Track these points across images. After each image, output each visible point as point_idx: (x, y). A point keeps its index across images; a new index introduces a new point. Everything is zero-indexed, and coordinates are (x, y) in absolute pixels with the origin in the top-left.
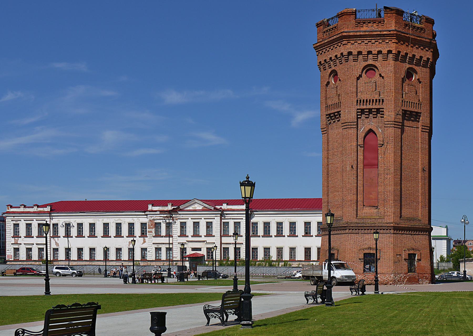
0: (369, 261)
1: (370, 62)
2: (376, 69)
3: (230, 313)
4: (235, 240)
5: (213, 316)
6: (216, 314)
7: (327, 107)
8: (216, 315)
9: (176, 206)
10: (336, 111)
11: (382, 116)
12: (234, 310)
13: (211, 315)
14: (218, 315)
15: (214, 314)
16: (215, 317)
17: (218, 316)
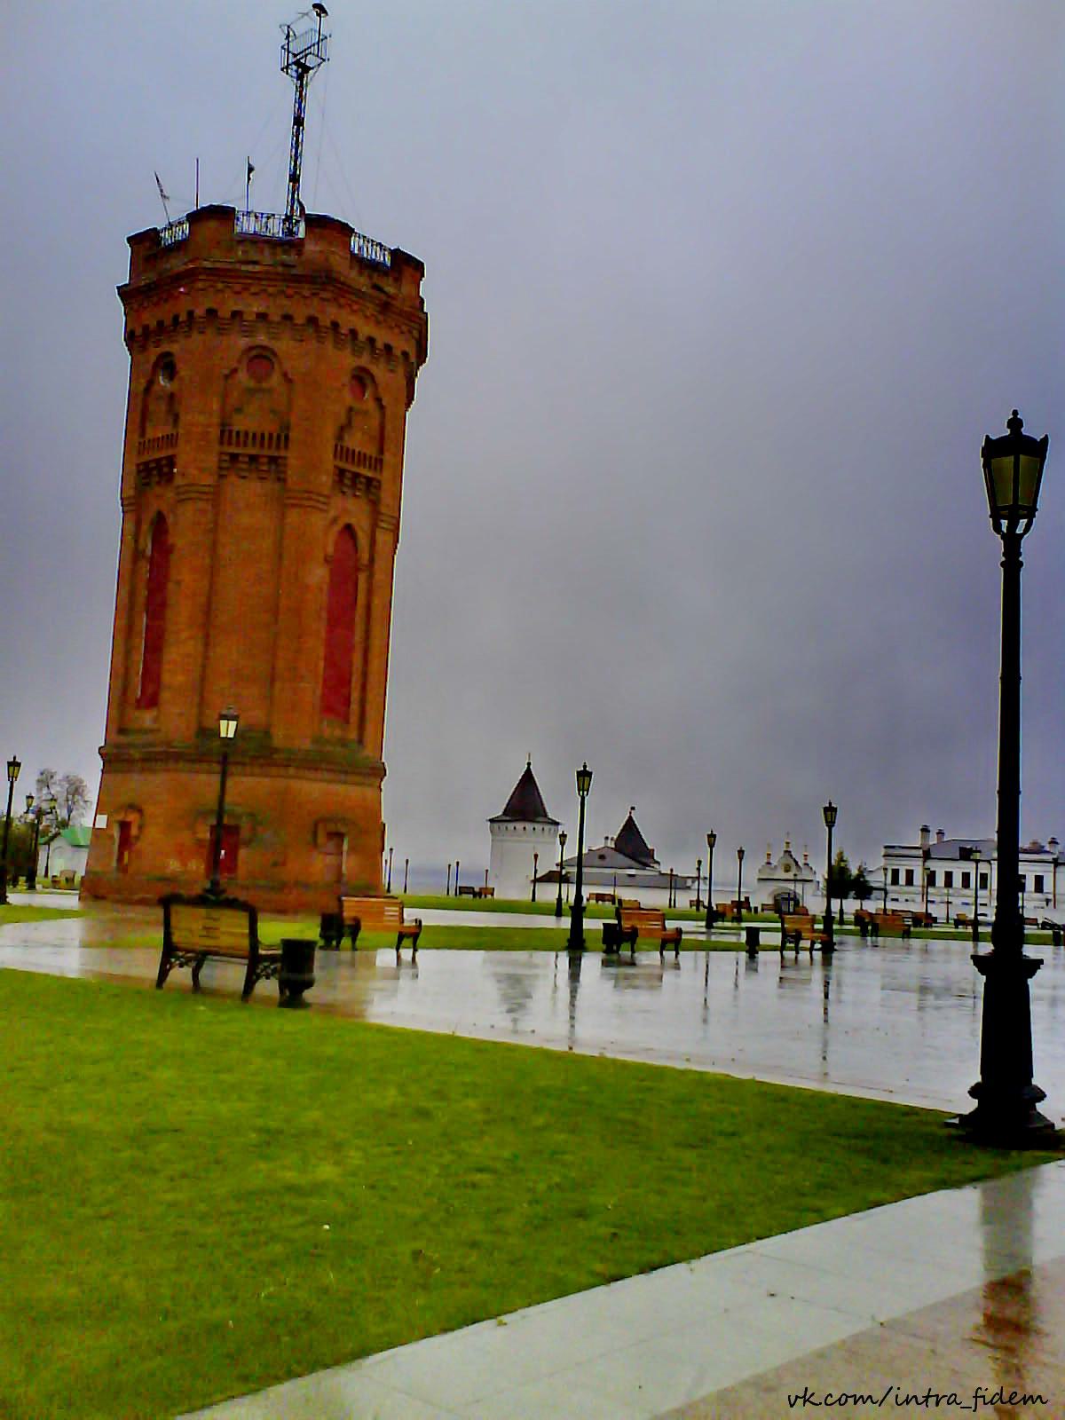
1: (262, 339)
2: (368, 382)
7: (143, 448)
10: (164, 454)
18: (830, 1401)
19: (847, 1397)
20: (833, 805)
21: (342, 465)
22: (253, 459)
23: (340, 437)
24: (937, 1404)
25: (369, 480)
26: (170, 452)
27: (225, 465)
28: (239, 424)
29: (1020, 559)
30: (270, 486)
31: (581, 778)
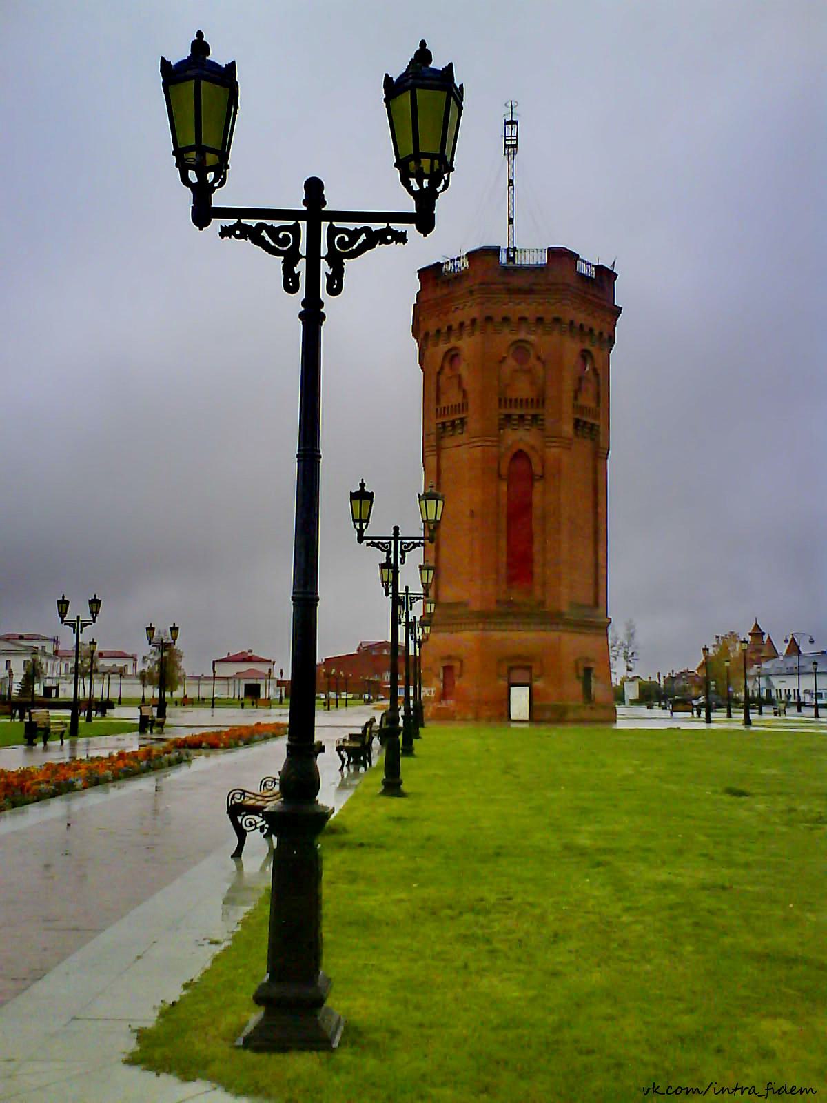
1: (522, 335)
2: (528, 347)
4: (358, 524)
7: (439, 414)
9: (248, 905)
10: (457, 416)
11: (541, 427)
18: (670, 1091)
19: (682, 1089)
20: (97, 598)
21: (507, 411)
22: (522, 417)
23: (576, 398)
24: (742, 1094)
25: (593, 425)
26: (462, 416)
27: (502, 422)
28: (581, 401)
29: (303, 309)
30: (588, 443)
31: (60, 605)
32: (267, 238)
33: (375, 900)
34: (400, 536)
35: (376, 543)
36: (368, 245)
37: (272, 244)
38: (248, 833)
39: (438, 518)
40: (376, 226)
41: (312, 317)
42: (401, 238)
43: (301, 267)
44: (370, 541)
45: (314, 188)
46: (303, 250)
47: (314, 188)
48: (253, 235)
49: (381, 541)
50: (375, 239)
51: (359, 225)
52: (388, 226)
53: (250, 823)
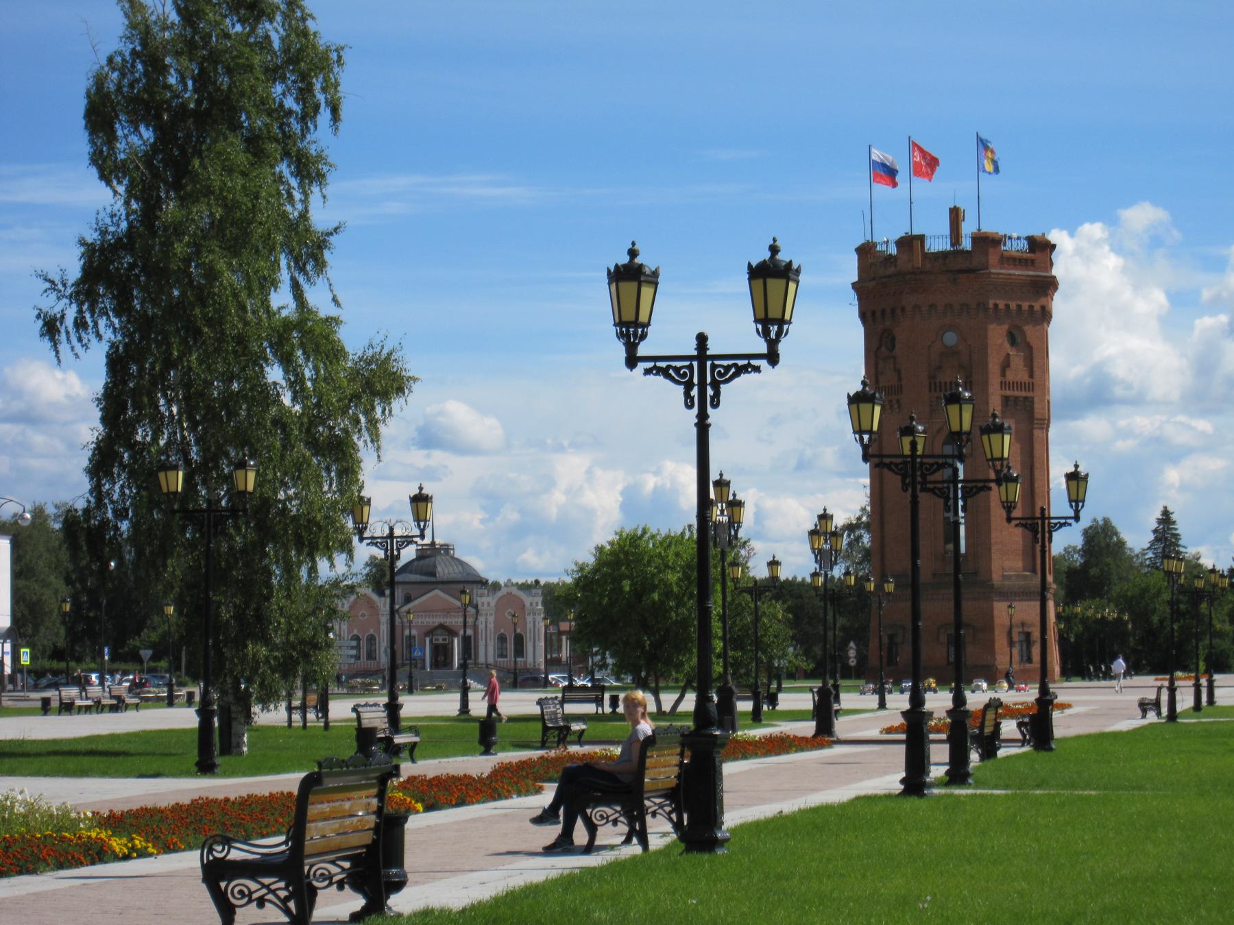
0: (301, 460)
3: (324, 880)
5: (251, 893)
6: (267, 887)
8: (657, 808)
12: (347, 865)
13: (319, 872)
14: (273, 892)
15: (253, 886)
16: (261, 902)
17: (277, 897)
23: (1003, 374)
25: (1026, 398)
28: (1010, 376)
32: (673, 374)
33: (744, 859)
34: (708, 353)
35: (662, 367)
36: (736, 375)
37: (677, 378)
38: (599, 828)
39: (985, 438)
40: (741, 363)
41: (702, 418)
42: (1070, 525)
43: (695, 392)
44: (650, 365)
45: (702, 339)
46: (696, 380)
47: (702, 339)
48: (664, 372)
49: (674, 364)
50: (740, 370)
51: (730, 362)
52: (749, 363)
53: (602, 816)
